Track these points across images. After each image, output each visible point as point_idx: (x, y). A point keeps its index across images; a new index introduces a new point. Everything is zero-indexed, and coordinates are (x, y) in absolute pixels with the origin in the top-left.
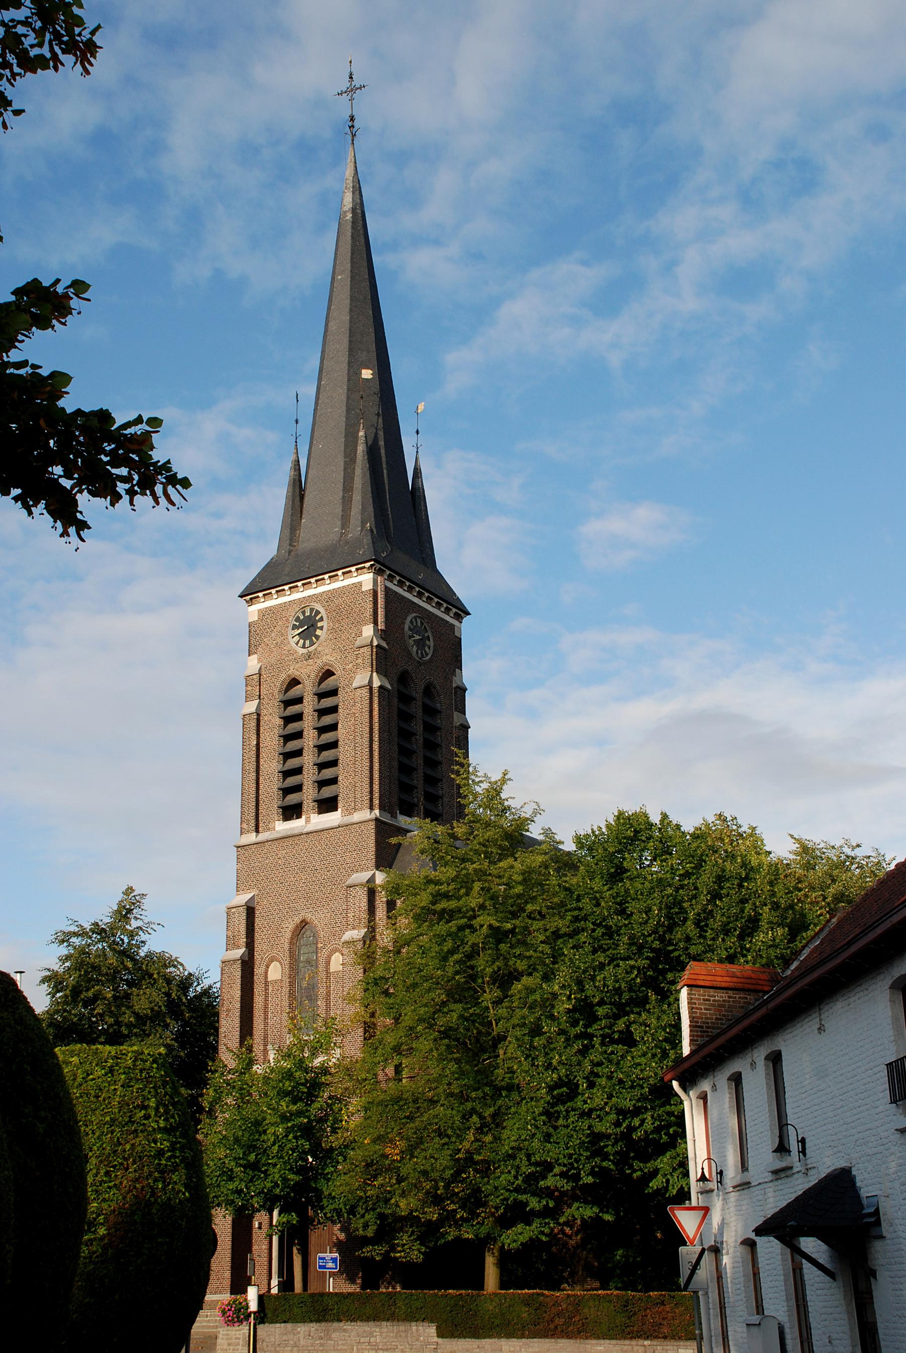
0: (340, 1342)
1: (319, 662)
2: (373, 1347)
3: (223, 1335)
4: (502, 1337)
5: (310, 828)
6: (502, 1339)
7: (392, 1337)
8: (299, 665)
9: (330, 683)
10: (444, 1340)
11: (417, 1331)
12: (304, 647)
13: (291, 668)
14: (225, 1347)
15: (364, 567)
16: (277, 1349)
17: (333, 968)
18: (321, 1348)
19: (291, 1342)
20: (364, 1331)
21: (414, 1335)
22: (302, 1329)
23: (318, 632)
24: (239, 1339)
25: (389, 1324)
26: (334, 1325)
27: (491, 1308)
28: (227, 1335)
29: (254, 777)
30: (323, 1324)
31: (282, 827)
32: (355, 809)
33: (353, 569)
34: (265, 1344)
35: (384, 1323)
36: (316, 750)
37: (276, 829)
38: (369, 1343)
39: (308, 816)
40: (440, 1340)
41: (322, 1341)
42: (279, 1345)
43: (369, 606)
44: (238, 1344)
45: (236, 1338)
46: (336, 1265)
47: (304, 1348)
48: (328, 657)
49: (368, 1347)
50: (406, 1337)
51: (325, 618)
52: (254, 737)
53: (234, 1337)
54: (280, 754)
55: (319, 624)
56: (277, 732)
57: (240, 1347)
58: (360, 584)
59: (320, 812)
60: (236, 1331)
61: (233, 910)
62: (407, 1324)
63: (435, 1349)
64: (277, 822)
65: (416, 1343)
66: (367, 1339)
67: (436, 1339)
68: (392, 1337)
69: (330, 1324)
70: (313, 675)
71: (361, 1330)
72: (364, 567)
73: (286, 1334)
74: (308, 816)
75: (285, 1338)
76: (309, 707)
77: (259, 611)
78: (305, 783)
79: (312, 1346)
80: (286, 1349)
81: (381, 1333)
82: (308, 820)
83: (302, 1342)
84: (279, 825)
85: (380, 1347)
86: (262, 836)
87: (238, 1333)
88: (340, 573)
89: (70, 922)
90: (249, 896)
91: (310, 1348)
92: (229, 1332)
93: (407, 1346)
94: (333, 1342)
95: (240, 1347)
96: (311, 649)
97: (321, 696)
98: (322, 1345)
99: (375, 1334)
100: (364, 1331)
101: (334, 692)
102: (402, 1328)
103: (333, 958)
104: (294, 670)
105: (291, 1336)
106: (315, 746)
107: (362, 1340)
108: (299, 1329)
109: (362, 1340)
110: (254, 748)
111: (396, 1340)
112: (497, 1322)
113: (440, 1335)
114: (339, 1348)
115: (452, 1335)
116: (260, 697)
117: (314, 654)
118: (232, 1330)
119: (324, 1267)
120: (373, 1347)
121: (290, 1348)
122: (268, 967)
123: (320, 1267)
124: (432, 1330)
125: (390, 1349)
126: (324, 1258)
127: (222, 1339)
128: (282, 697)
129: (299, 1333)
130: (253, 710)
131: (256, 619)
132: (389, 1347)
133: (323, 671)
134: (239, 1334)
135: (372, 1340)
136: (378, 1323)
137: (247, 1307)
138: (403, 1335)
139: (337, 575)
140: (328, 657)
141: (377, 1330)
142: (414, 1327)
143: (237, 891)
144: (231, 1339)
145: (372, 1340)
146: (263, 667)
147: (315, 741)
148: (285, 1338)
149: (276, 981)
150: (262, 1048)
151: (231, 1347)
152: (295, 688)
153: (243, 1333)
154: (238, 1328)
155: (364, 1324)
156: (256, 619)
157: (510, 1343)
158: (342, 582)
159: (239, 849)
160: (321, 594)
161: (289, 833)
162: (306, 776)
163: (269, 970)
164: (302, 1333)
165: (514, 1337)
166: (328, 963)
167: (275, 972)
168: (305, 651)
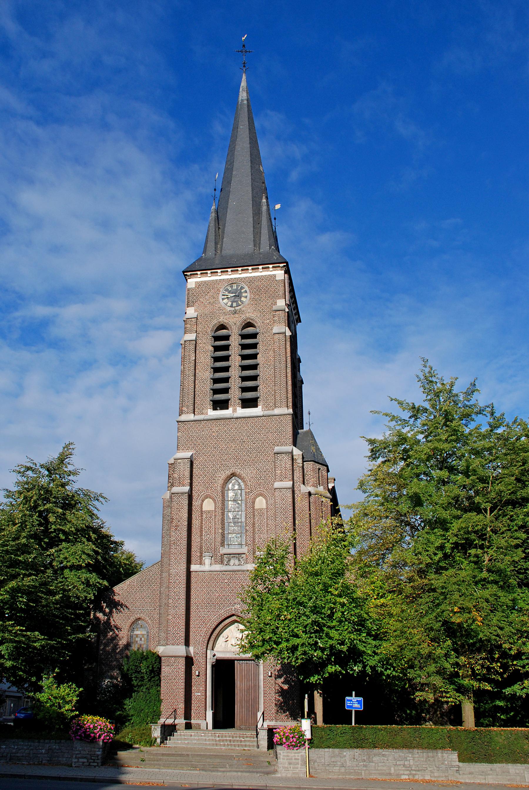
0: (380, 764)
1: (243, 316)
2: (407, 769)
3: (284, 756)
4: (509, 763)
5: (236, 415)
6: (509, 764)
7: (423, 761)
8: (228, 316)
9: (250, 330)
10: (464, 764)
11: (442, 756)
12: (232, 306)
13: (222, 318)
14: (286, 766)
15: (279, 267)
16: (327, 768)
17: (257, 506)
18: (365, 768)
19: (339, 763)
20: (400, 756)
21: (440, 760)
22: (348, 753)
23: (243, 299)
24: (298, 759)
25: (419, 751)
26: (374, 751)
27: (501, 740)
28: (288, 756)
29: (193, 379)
30: (365, 750)
31: (212, 413)
32: (275, 407)
33: (271, 266)
34: (316, 764)
35: (416, 751)
36: (240, 368)
37: (208, 414)
38: (404, 765)
39: (235, 408)
40: (461, 764)
41: (365, 763)
42: (328, 765)
43: (282, 289)
44: (298, 764)
45: (295, 759)
46: (361, 706)
47: (350, 768)
48: (250, 314)
49: (403, 768)
50: (434, 761)
51: (248, 291)
52: (193, 355)
53: (293, 758)
54: (212, 368)
55: (244, 295)
56: (209, 354)
57: (299, 766)
58: (275, 276)
59: (243, 407)
60: (295, 753)
61: (179, 461)
62: (435, 751)
63: (457, 770)
64: (209, 410)
65: (442, 766)
66: (402, 763)
67: (457, 763)
68: (423, 761)
69: (371, 750)
70: (238, 324)
71: (397, 755)
72: (279, 267)
73: (334, 757)
74: (235, 408)
75: (333, 759)
76: (235, 342)
77: (196, 282)
78: (233, 387)
79: (357, 766)
80: (335, 768)
81: (414, 758)
82: (235, 411)
83: (348, 763)
84: (210, 411)
85: (413, 768)
86: (197, 417)
87: (296, 755)
88: (260, 267)
89: (28, 460)
90: (190, 454)
91: (355, 768)
92: (289, 754)
93: (435, 768)
94: (374, 764)
95: (299, 766)
96: (236, 308)
97: (244, 337)
98: (365, 766)
99: (408, 758)
100: (400, 756)
101: (254, 336)
102: (430, 754)
103: (257, 500)
104: (223, 319)
105: (338, 759)
106: (240, 366)
107: (398, 763)
108: (345, 754)
109: (398, 763)
110: (193, 362)
111: (426, 763)
112: (506, 751)
113: (461, 759)
114: (379, 768)
115: (470, 760)
116: (196, 332)
117: (239, 311)
118: (292, 753)
119: (351, 707)
120: (407, 769)
121: (338, 768)
122: (203, 501)
123: (348, 706)
124: (455, 756)
125: (421, 770)
126: (351, 700)
127: (284, 759)
128: (213, 334)
129: (345, 756)
130: (194, 338)
131: (194, 287)
132: (421, 768)
133: (246, 322)
134: (298, 756)
135: (406, 763)
136: (411, 750)
137: (303, 735)
138: (432, 759)
139: (258, 269)
140: (250, 314)
141: (410, 755)
142: (440, 753)
143: (178, 450)
144: (292, 759)
145: (406, 763)
146: (198, 315)
147: (240, 363)
148: (333, 759)
149: (209, 512)
150: (199, 554)
151: (292, 766)
152: (221, 331)
153: (301, 755)
154: (296, 751)
155: (400, 751)
156: (194, 287)
157: (515, 767)
158: (261, 273)
159: (180, 423)
160: (245, 278)
161: (222, 417)
162: (233, 383)
163: (204, 503)
164: (347, 756)
165: (518, 763)
166: (254, 503)
167: (208, 505)
168: (233, 309)
